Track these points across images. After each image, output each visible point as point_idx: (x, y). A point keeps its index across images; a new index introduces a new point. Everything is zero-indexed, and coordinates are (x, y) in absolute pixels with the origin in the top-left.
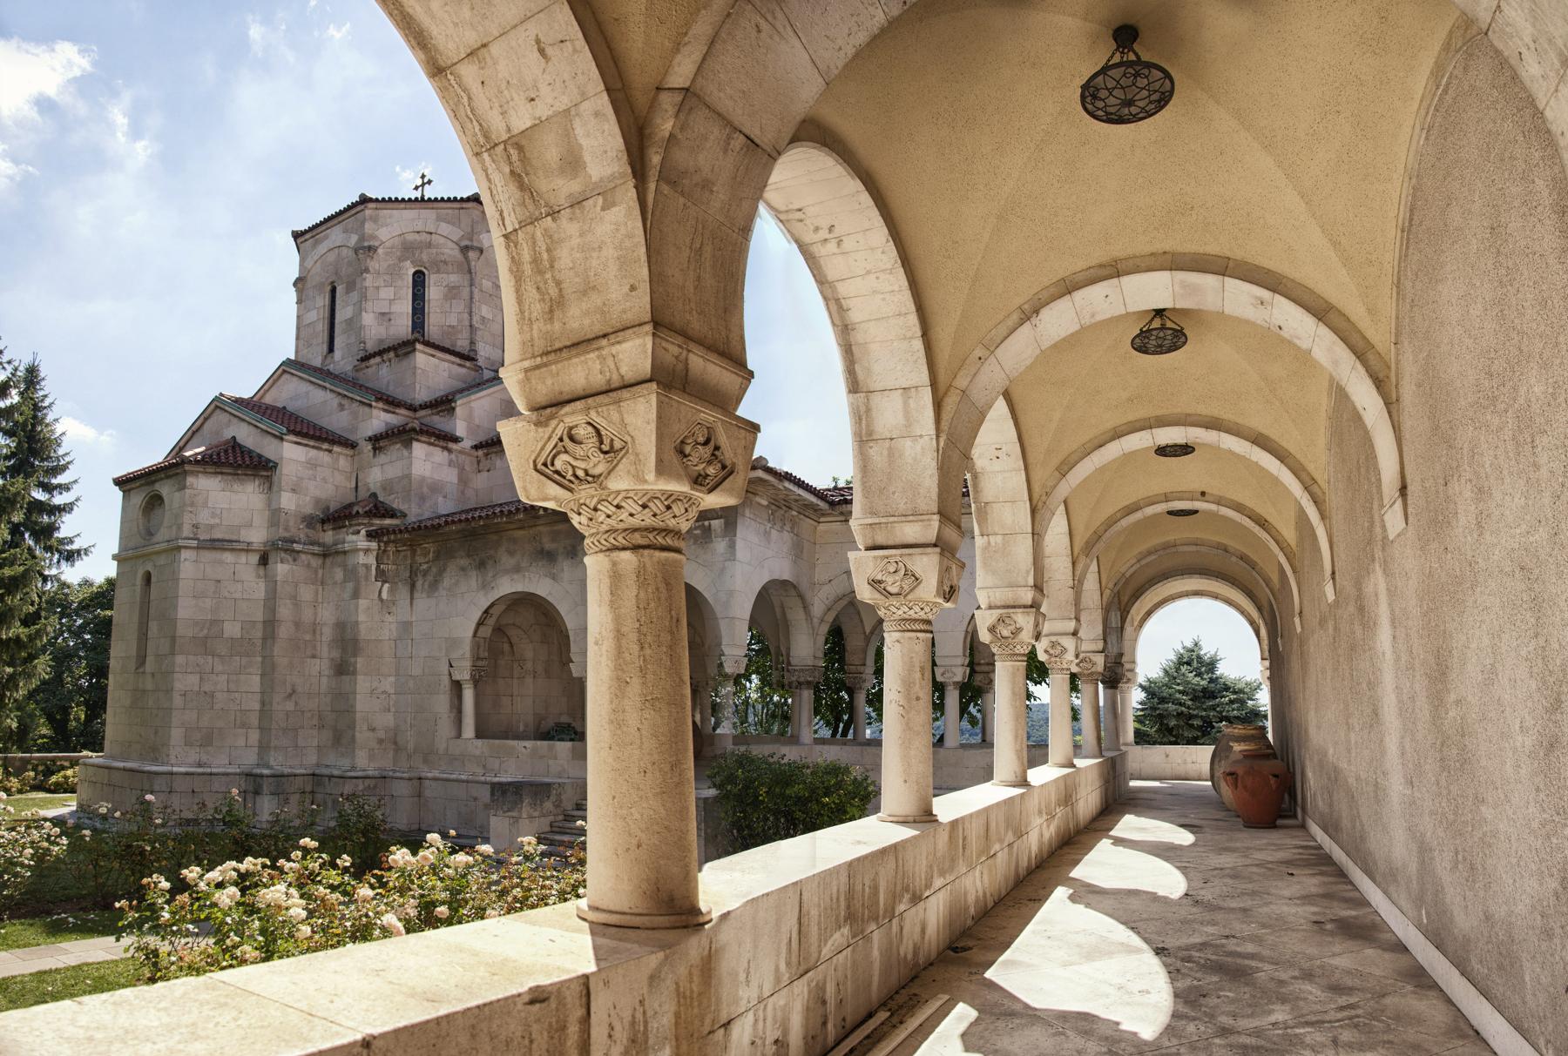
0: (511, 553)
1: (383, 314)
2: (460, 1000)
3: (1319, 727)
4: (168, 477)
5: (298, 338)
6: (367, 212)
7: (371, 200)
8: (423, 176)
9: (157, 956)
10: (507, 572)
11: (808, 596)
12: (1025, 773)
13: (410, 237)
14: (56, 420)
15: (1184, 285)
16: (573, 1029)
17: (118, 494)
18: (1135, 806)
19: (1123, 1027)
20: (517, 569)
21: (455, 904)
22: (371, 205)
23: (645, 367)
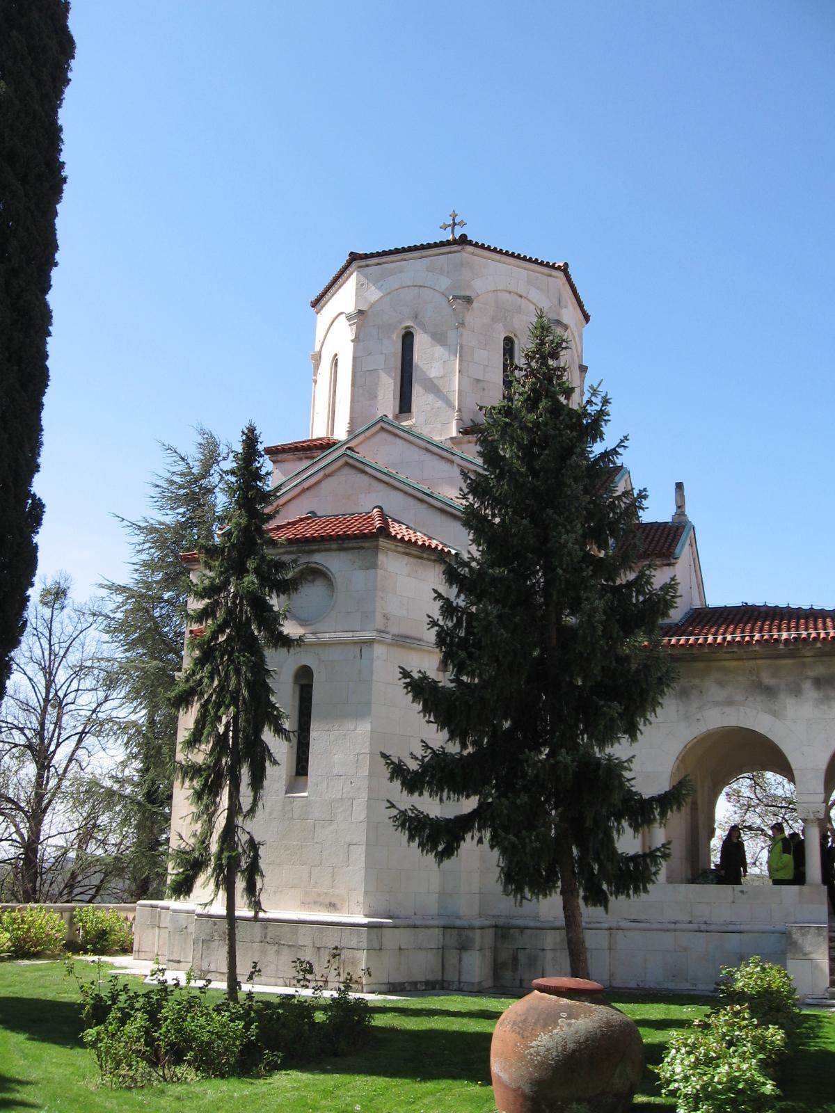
0: (721, 684)
1: (478, 381)
2: (448, 1000)
3: (473, 254)
4: (341, 549)
5: (353, 385)
6: (464, 255)
7: (470, 243)
8: (454, 216)
9: (400, 272)
10: (717, 704)
11: (98, 898)
12: (398, 809)
13: (505, 297)
14: (427, 747)
15: (576, 981)
16: (598, 925)
17: (352, 344)
18: (663, 682)
19: (8, 682)
20: (730, 703)
21: (152, 896)
22: (470, 249)
23: (403, 809)
